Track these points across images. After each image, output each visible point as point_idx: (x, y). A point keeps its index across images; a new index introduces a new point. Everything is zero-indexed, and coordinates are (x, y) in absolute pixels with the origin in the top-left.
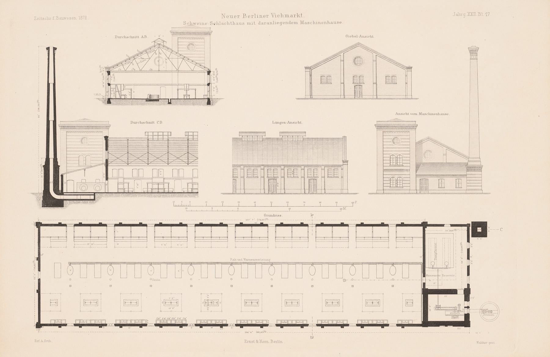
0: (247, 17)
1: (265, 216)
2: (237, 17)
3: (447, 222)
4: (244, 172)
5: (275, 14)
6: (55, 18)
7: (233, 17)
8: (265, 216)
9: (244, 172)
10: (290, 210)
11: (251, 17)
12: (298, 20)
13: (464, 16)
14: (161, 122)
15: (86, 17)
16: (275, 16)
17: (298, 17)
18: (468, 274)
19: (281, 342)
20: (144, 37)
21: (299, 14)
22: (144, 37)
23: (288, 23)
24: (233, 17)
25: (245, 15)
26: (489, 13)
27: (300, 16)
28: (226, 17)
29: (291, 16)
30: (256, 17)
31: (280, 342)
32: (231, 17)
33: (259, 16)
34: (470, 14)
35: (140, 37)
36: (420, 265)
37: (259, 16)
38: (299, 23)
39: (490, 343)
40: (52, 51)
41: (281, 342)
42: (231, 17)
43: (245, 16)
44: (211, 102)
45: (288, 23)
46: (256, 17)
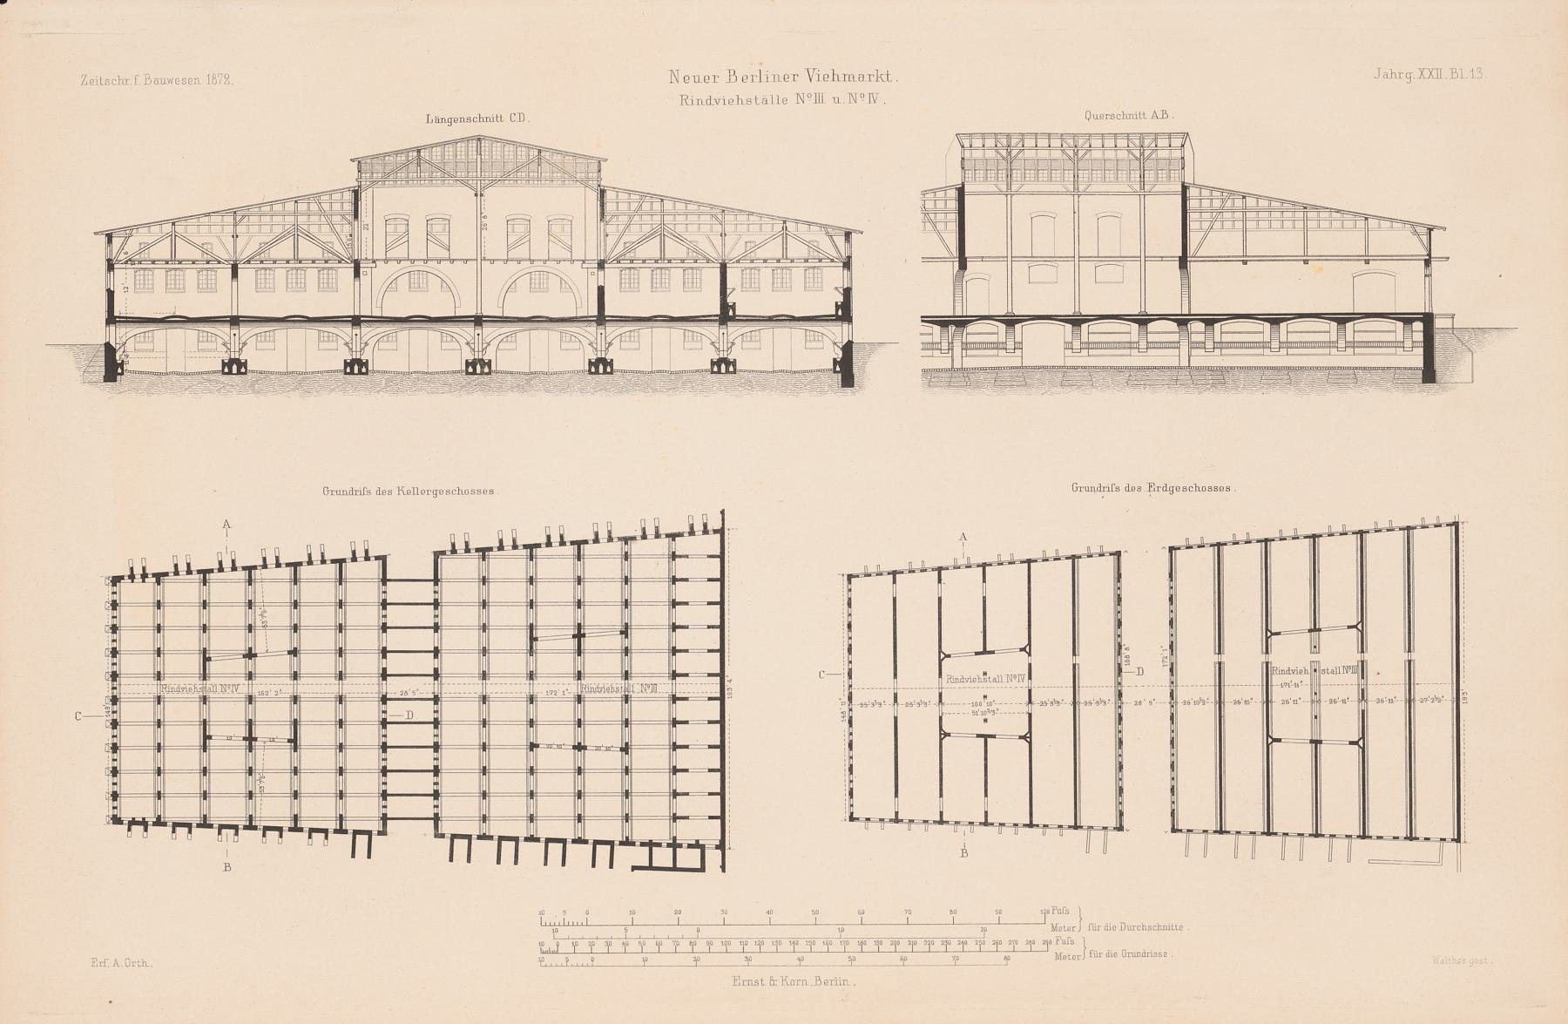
0: (739, 79)
3: (1069, 660)
5: (816, 71)
6: (141, 80)
10: (958, 963)
11: (750, 78)
13: (1409, 81)
14: (410, 713)
15: (227, 77)
17: (879, 79)
18: (941, 796)
20: (1160, 115)
21: (883, 71)
22: (1160, 115)
23: (704, 103)
24: (702, 79)
25: (732, 73)
26: (85, 83)
27: (885, 77)
28: (681, 79)
29: (861, 79)
34: (1426, 73)
35: (1149, 114)
36: (288, 727)
38: (792, 99)
40: (722, 512)
43: (733, 78)
45: (704, 103)
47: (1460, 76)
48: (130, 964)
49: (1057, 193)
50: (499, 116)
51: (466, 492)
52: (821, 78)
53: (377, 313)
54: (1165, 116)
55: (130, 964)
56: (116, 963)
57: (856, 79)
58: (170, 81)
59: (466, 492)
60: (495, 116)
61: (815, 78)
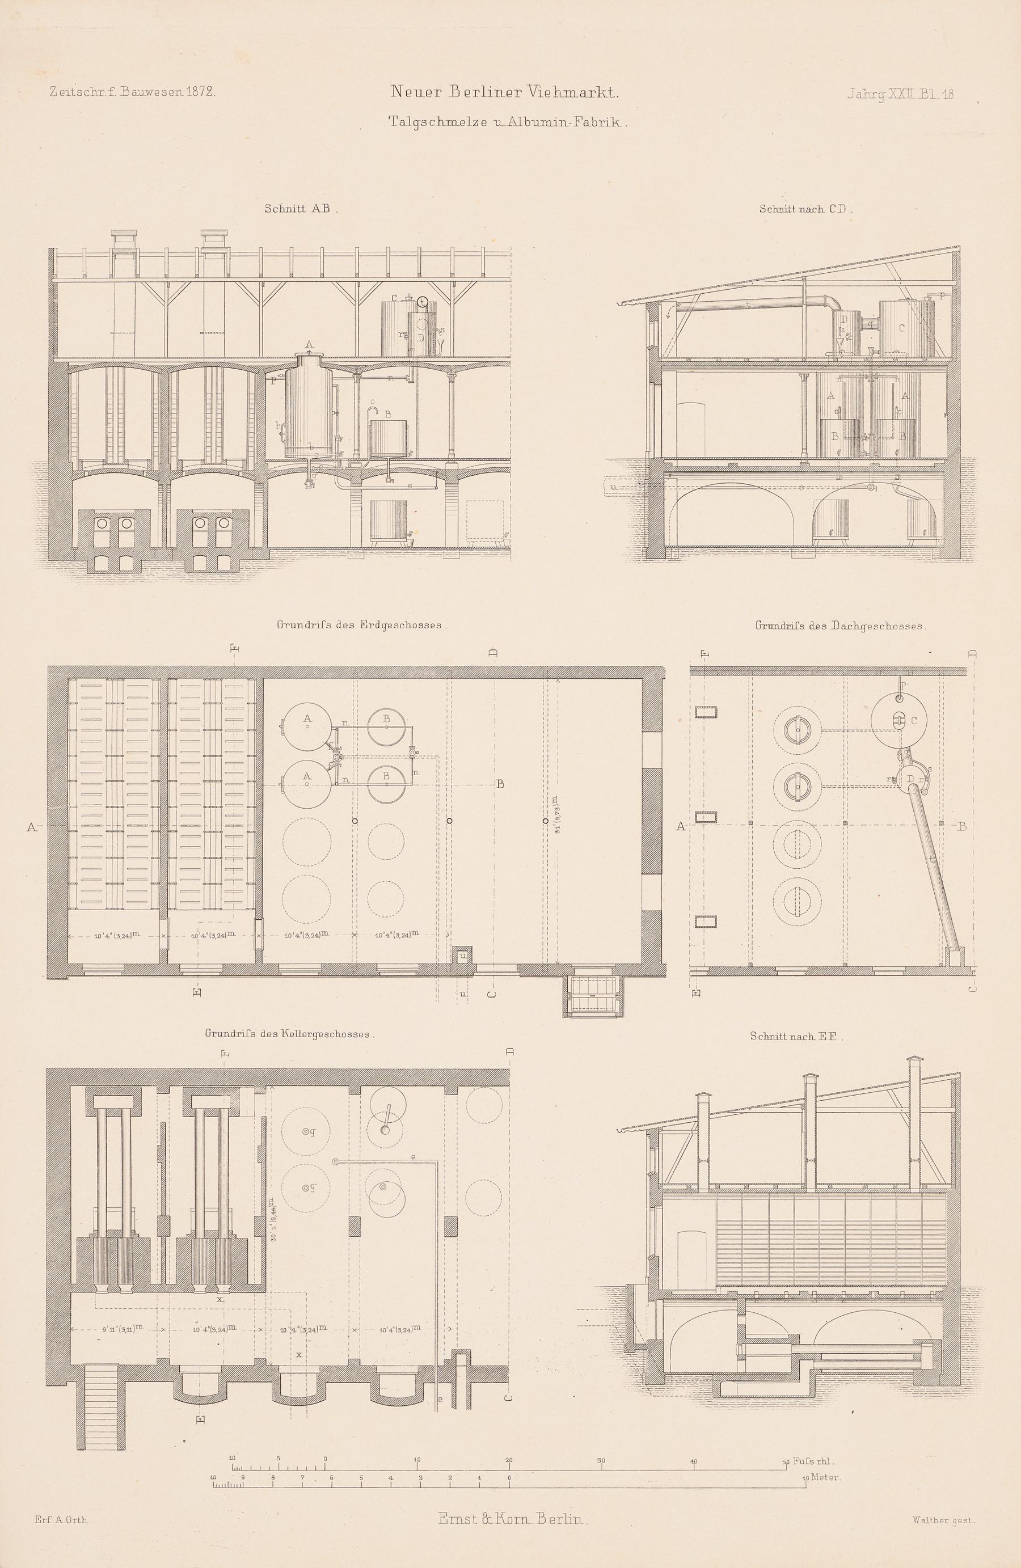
0: (462, 94)
1: (280, 626)
2: (434, 93)
4: (704, 708)
7: (424, 94)
8: (280, 626)
9: (704, 708)
11: (473, 93)
12: (943, 309)
16: (537, 94)
19: (578, 1520)
20: (321, 209)
21: (605, 88)
22: (321, 209)
24: (424, 94)
26: (54, 94)
27: (607, 94)
28: (403, 94)
29: (583, 95)
30: (487, 93)
31: (573, 1520)
32: (419, 95)
33: (494, 93)
35: (309, 208)
37: (494, 93)
39: (956, 1521)
41: (578, 1520)
42: (419, 95)
43: (456, 93)
44: (628, 479)
46: (487, 93)
47: (930, 96)
48: (70, 1520)
49: (463, 460)
50: (301, 206)
51: (344, 1035)
52: (543, 94)
53: (115, 682)
54: (327, 209)
55: (70, 1520)
56: (59, 1520)
57: (414, 92)
58: (149, 93)
59: (344, 1035)
60: (296, 207)
61: (537, 94)
